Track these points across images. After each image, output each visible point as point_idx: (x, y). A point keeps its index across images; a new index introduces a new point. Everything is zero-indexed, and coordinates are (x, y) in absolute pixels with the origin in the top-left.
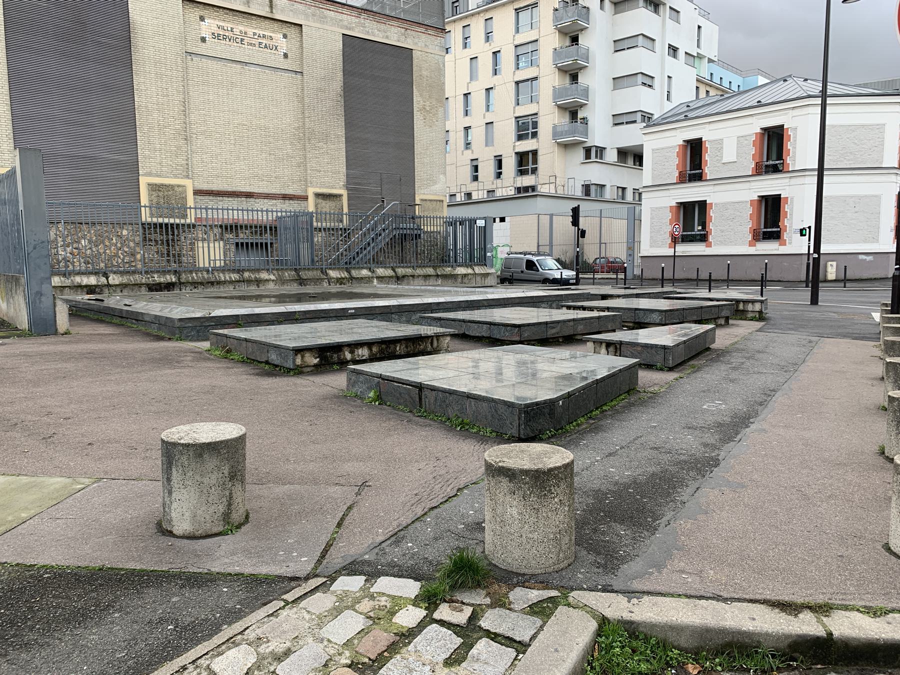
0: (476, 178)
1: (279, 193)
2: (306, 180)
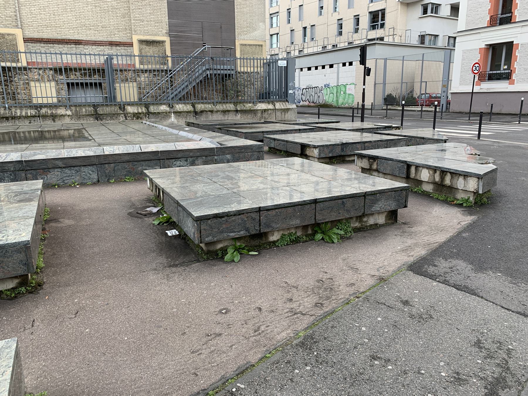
0: (340, 34)
1: (106, 40)
2: (131, 29)
